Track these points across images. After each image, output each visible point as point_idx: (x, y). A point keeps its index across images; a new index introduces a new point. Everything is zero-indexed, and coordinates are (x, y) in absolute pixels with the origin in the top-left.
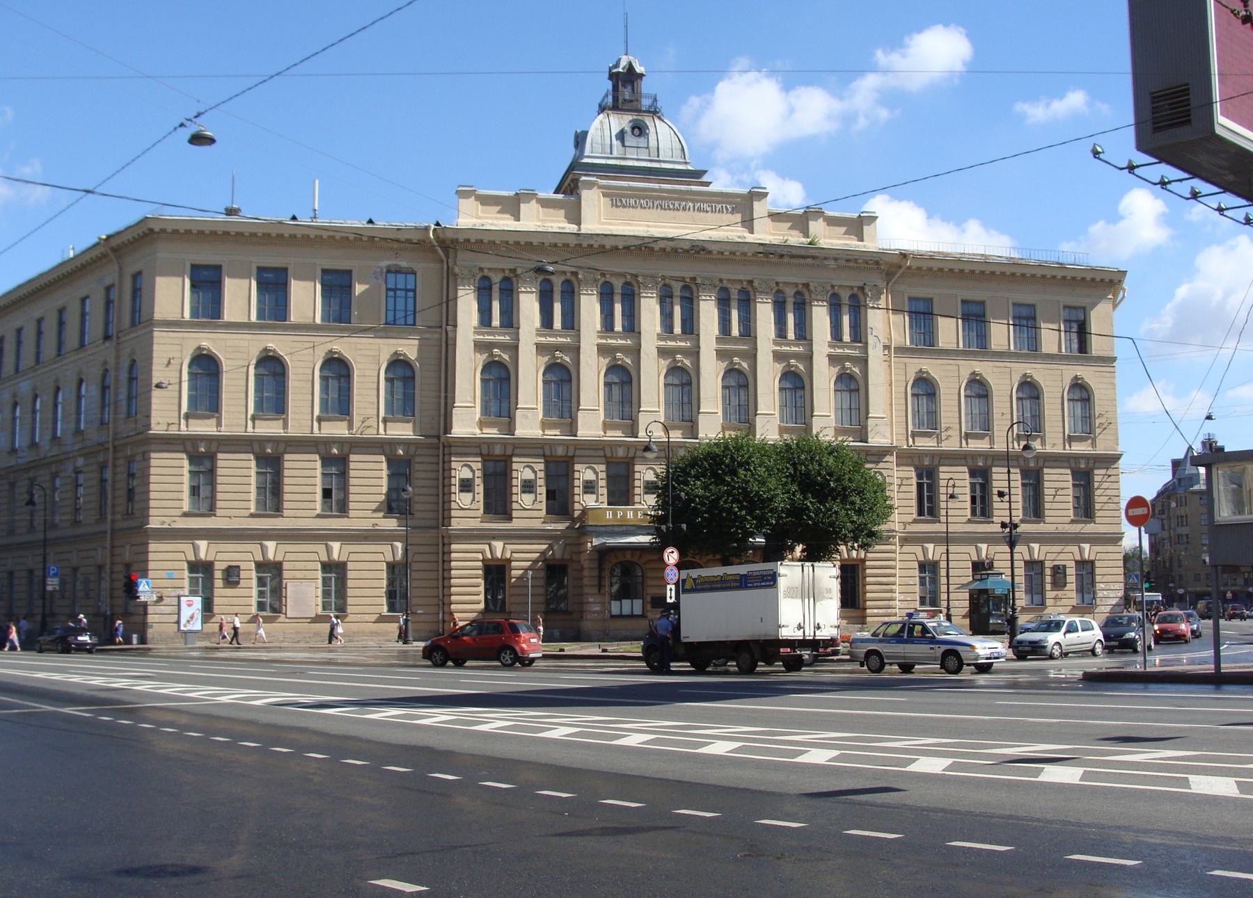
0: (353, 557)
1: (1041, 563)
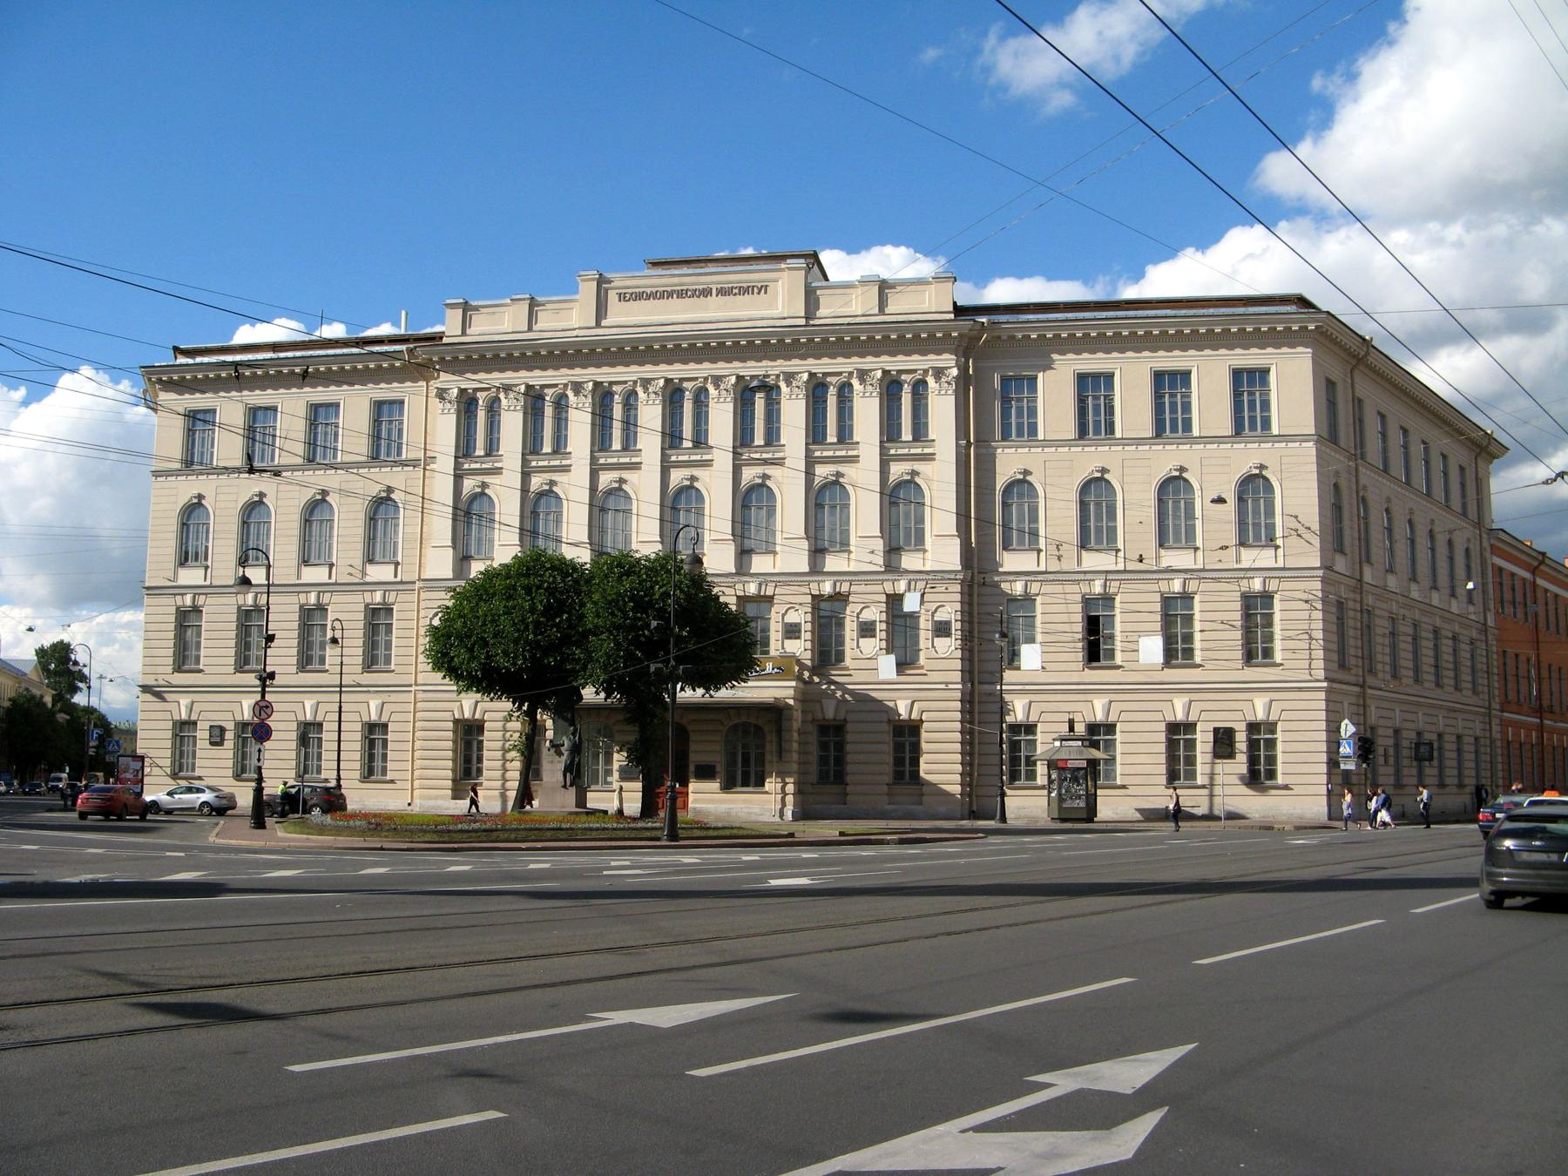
1: (1190, 727)
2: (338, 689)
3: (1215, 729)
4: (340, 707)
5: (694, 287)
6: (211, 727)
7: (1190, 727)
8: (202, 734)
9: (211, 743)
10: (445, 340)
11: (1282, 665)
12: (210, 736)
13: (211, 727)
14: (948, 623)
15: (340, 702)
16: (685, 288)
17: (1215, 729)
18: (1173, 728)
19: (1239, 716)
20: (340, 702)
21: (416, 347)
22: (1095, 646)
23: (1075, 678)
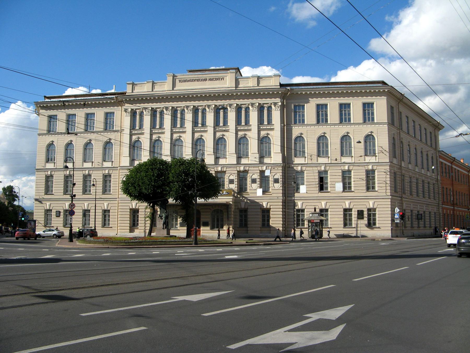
0: (378, 206)
1: (350, 210)
2: (95, 200)
3: (358, 210)
4: (95, 205)
5: (202, 78)
6: (56, 211)
7: (350, 210)
8: (54, 213)
9: (56, 216)
10: (127, 94)
11: (378, 191)
12: (56, 214)
13: (56, 211)
14: (278, 179)
15: (95, 204)
16: (199, 78)
17: (358, 210)
18: (345, 210)
19: (365, 206)
20: (95, 204)
21: (118, 96)
22: (322, 186)
23: (316, 195)
